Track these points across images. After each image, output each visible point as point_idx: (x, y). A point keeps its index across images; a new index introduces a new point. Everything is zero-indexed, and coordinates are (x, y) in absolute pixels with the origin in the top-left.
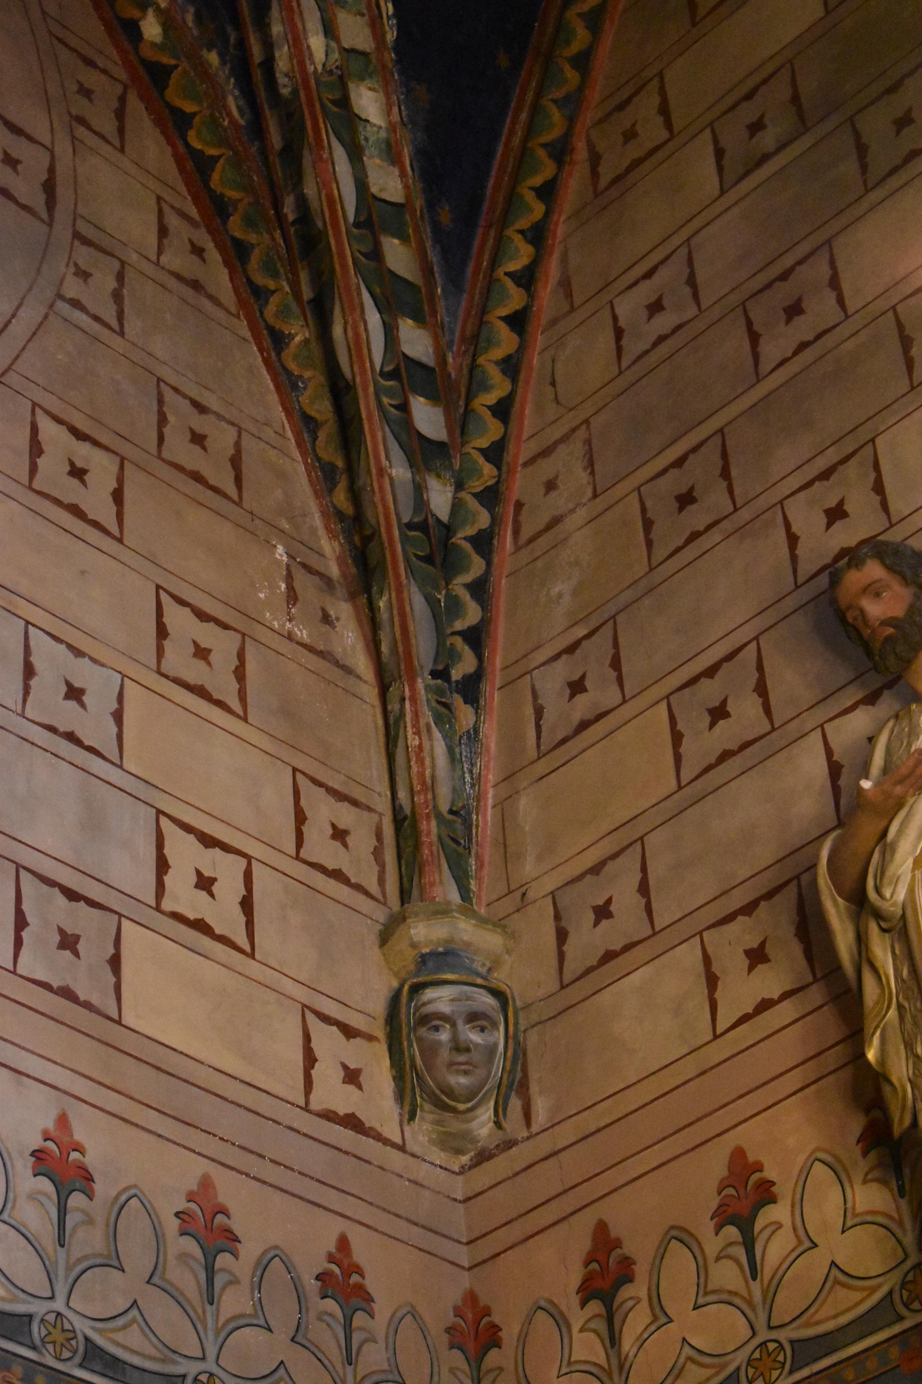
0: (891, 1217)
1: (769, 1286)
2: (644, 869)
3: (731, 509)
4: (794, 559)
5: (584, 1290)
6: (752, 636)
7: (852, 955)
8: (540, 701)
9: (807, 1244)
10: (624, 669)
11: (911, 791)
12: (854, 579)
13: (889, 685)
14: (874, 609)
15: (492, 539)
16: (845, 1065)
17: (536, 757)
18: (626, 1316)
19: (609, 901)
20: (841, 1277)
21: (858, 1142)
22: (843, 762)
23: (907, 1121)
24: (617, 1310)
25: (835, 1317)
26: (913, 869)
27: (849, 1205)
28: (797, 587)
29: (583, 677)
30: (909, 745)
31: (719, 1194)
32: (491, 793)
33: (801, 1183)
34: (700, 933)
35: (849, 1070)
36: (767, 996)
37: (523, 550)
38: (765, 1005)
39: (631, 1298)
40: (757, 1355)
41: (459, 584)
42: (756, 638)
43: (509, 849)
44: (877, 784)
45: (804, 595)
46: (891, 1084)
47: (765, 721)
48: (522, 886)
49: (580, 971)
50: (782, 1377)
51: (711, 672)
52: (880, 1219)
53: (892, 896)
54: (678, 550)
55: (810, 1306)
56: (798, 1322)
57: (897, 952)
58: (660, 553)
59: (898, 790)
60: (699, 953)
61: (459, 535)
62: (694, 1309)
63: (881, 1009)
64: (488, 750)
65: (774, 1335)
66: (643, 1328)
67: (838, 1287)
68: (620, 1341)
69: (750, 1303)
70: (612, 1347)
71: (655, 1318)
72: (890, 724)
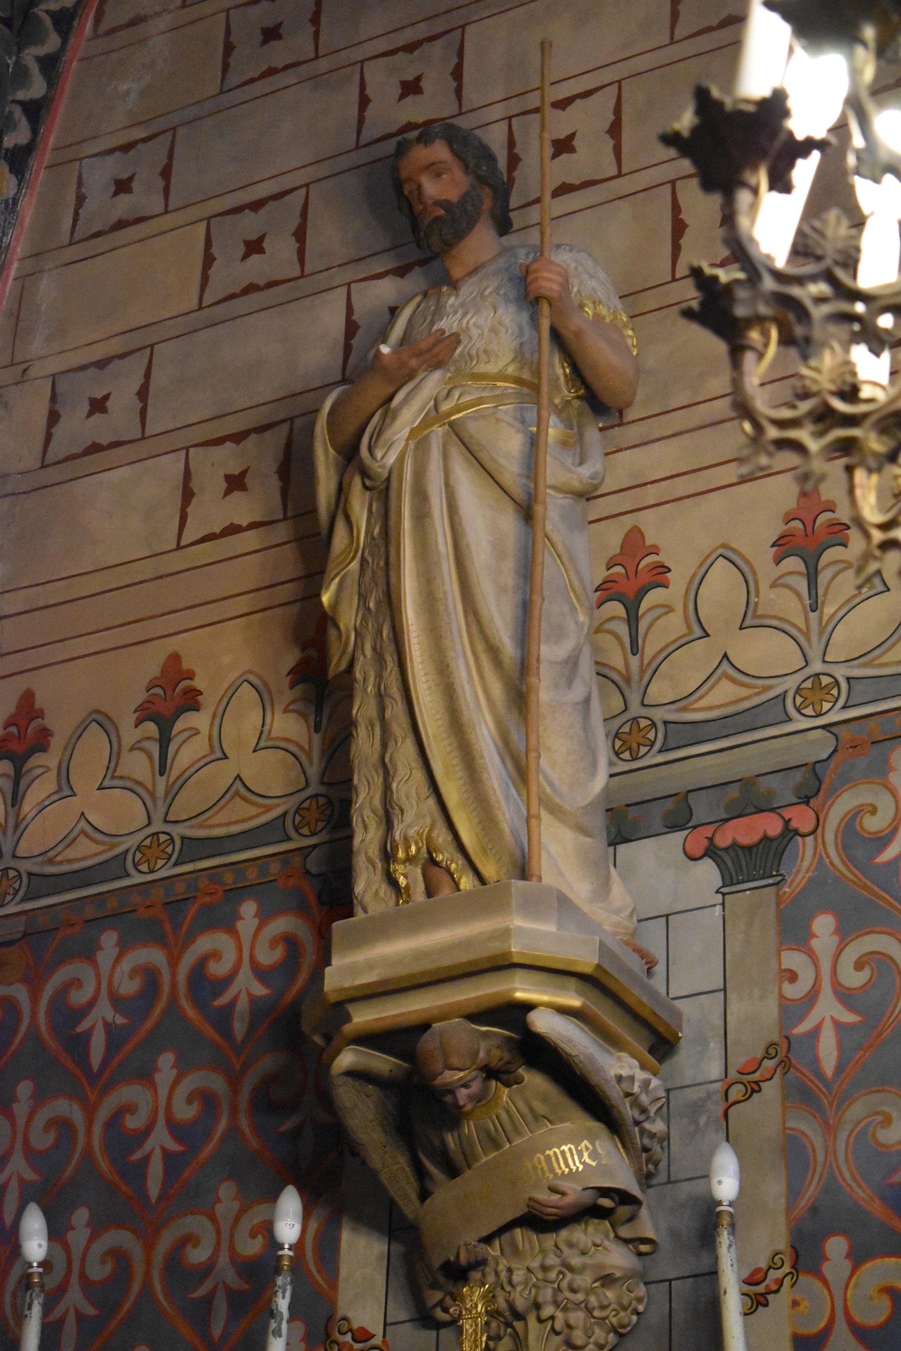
0: (301, 748)
1: (174, 783)
2: (148, 374)
3: (312, 55)
4: (361, 120)
5: (142, 710)
6: (302, 183)
7: (329, 503)
8: (83, 190)
9: (219, 754)
10: (173, 181)
11: (424, 366)
12: (422, 154)
13: (422, 263)
14: (431, 188)
15: (73, 19)
16: (294, 602)
17: (67, 242)
18: (33, 781)
19: (106, 397)
20: (243, 790)
21: (289, 673)
22: (360, 322)
23: (344, 666)
24: (26, 772)
25: (229, 824)
26: (407, 440)
27: (267, 727)
28: (358, 147)
29: (131, 179)
30: (432, 323)
31: (148, 691)
32: (15, 265)
33: (225, 700)
34: (187, 449)
35: (295, 609)
36: (237, 522)
37: (100, 40)
38: (233, 530)
39: (42, 766)
40: (147, 842)
41: (31, 55)
42: (307, 185)
43: (20, 324)
44: (395, 351)
45: (362, 156)
46: (338, 628)
47: (298, 266)
48: (27, 361)
49: (62, 456)
50: (13, 903)
51: (256, 206)
52: (291, 747)
53: (383, 458)
54: (253, 80)
55: (207, 810)
56: (193, 822)
57: (374, 509)
58: (234, 79)
59: (414, 362)
60: (182, 466)
61: (43, 7)
62: (98, 789)
63: (345, 559)
64: (22, 226)
65: (168, 828)
66: (46, 795)
67: (237, 799)
68: (21, 804)
69: (152, 795)
70: (13, 806)
71: (60, 790)
72: (418, 299)
